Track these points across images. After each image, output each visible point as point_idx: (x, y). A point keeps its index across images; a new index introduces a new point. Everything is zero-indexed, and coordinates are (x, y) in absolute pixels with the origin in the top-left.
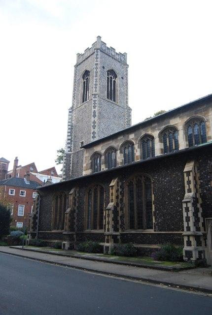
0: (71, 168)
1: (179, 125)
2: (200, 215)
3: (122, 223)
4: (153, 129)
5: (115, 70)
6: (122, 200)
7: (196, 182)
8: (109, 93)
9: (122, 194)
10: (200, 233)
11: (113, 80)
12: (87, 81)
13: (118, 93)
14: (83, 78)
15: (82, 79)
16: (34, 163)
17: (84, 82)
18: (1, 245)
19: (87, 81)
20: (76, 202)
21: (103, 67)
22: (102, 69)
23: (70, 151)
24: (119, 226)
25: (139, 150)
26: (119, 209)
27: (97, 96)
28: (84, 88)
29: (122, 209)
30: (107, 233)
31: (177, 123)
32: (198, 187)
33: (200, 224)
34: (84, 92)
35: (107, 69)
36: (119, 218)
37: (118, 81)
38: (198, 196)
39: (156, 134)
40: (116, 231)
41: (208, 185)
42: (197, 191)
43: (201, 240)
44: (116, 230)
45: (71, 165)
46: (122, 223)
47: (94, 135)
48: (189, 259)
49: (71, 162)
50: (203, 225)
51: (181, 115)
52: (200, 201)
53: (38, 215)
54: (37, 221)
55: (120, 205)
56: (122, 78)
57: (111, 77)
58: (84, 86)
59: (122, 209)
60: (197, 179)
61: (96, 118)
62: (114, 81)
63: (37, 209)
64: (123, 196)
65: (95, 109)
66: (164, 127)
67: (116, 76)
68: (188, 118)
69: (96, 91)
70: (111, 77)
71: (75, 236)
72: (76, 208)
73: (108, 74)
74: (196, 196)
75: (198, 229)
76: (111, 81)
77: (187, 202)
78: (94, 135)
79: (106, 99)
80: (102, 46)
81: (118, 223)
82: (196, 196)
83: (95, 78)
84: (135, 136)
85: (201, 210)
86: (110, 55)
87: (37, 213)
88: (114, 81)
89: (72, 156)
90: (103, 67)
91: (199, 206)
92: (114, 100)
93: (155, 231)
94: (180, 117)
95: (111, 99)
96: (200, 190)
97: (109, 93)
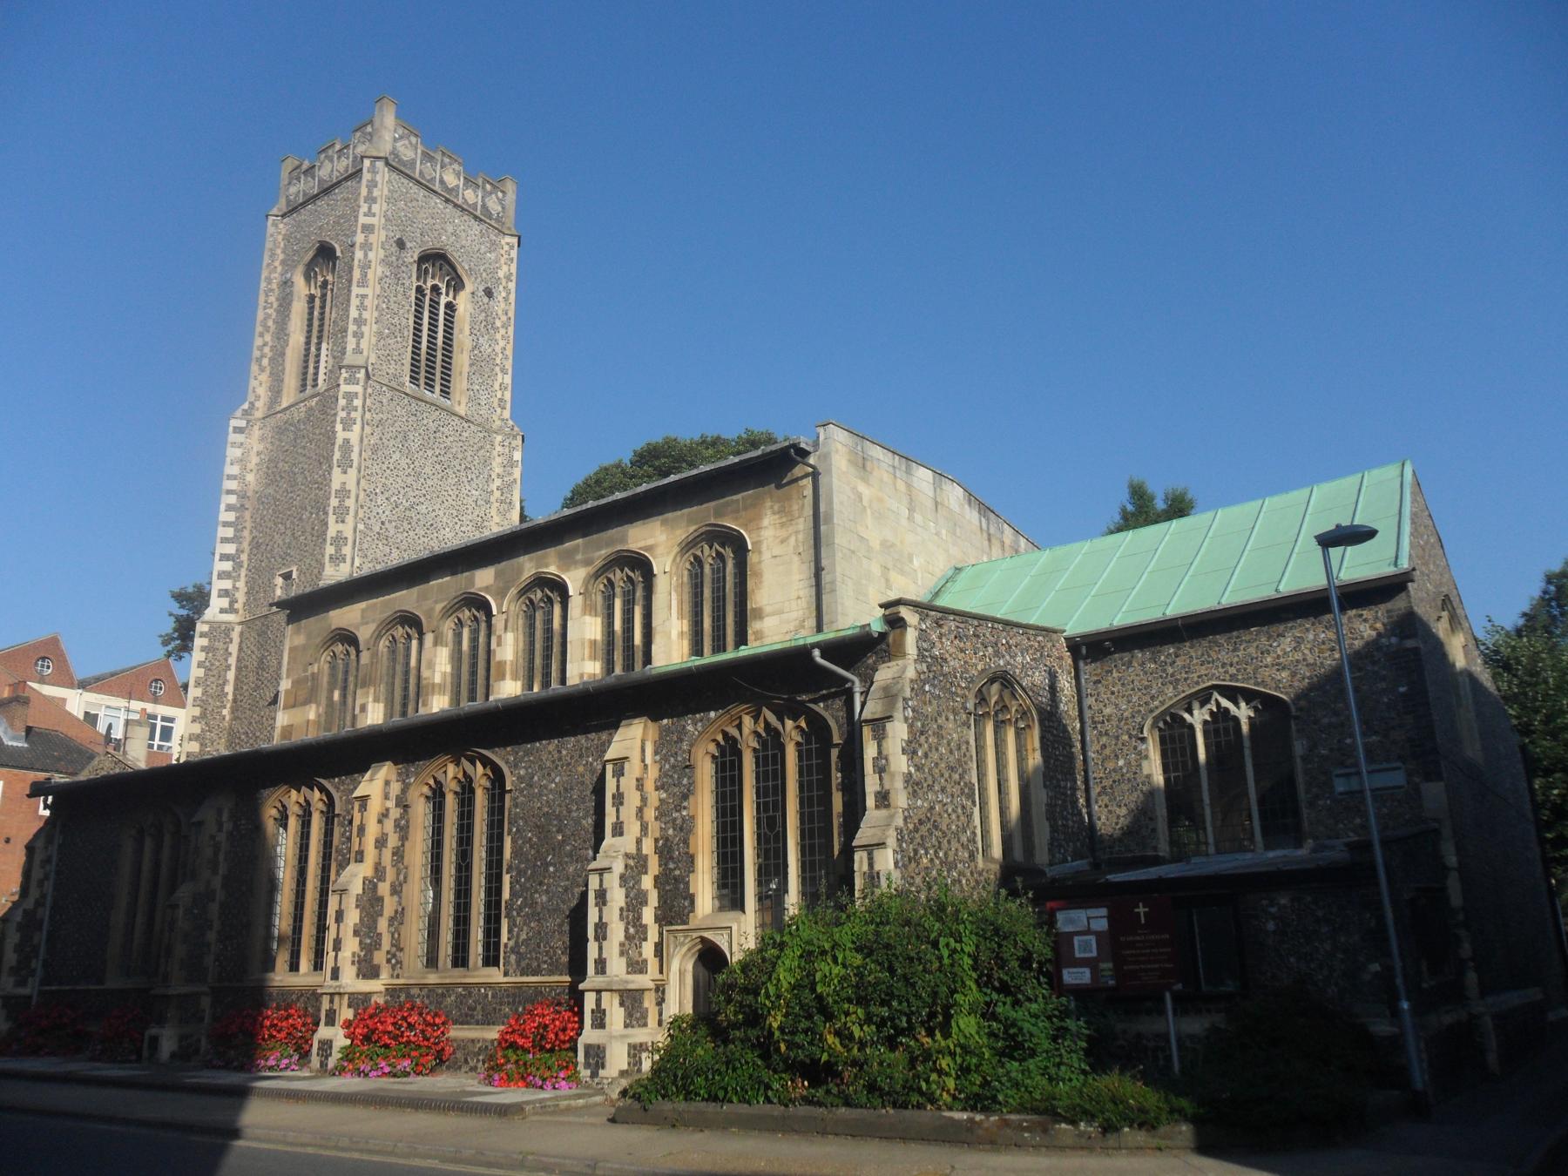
0: (229, 689)
1: (659, 551)
2: (648, 915)
3: (397, 946)
4: (568, 561)
5: (454, 255)
6: (398, 854)
7: (644, 800)
8: (423, 356)
9: (403, 829)
10: (644, 981)
11: (443, 300)
12: (324, 296)
13: (461, 360)
14: (308, 278)
15: (299, 280)
16: (54, 642)
17: (311, 298)
18: (2, 765)
19: (324, 296)
20: (221, 857)
21: (401, 244)
22: (395, 249)
23: (231, 610)
24: (380, 957)
25: (509, 638)
26: (384, 889)
27: (361, 375)
28: (310, 325)
29: (396, 890)
30: (330, 985)
31: (650, 542)
32: (650, 814)
33: (648, 949)
34: (308, 343)
35: (412, 256)
36: (383, 925)
37: (463, 302)
38: (648, 847)
39: (574, 580)
40: (365, 977)
41: (679, 811)
42: (644, 828)
43: (646, 1004)
44: (368, 969)
45: (231, 675)
46: (397, 946)
47: (338, 550)
48: (594, 1075)
49: (232, 661)
50: (659, 950)
51: (670, 515)
52: (654, 867)
53: (45, 913)
54: (41, 938)
55: (390, 874)
56: (489, 293)
57: (435, 289)
58: (311, 313)
59: (396, 890)
60: (649, 785)
61: (353, 473)
62: (449, 306)
63: (41, 883)
64: (404, 838)
65: (347, 435)
66: (604, 552)
67: (457, 284)
68: (692, 529)
69: (358, 351)
70: (435, 289)
71: (206, 1002)
72: (217, 883)
73: (422, 274)
74: (639, 849)
75: (637, 967)
76: (434, 305)
77: (601, 872)
78: (338, 550)
79: (409, 387)
80: (399, 144)
81: (377, 945)
82: (639, 849)
83: (355, 290)
84: (497, 576)
85: (653, 899)
86: (437, 187)
87: (39, 903)
88: (449, 306)
89: (235, 636)
90: (401, 244)
91: (647, 882)
92: (445, 392)
93: (506, 974)
94: (664, 523)
95: (430, 387)
96: (654, 828)
97: (423, 356)
